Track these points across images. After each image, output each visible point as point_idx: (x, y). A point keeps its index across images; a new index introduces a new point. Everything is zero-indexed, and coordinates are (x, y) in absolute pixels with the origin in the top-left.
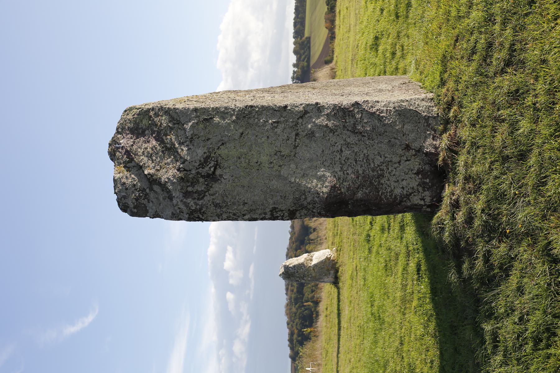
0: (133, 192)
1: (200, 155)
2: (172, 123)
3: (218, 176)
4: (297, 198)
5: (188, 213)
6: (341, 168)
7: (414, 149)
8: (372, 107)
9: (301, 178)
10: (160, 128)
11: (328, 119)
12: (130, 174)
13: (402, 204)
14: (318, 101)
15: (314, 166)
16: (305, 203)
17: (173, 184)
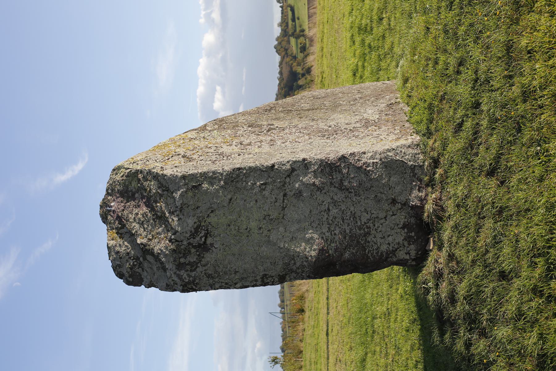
0: (127, 261)
1: (190, 225)
2: (161, 189)
3: (209, 245)
4: (287, 263)
5: (181, 285)
6: (329, 228)
7: (401, 203)
8: (359, 160)
9: (290, 243)
10: (150, 194)
11: (316, 177)
12: (123, 242)
13: (388, 260)
14: (306, 157)
15: (302, 228)
16: (294, 268)
17: (166, 256)
